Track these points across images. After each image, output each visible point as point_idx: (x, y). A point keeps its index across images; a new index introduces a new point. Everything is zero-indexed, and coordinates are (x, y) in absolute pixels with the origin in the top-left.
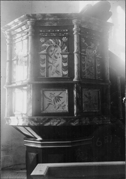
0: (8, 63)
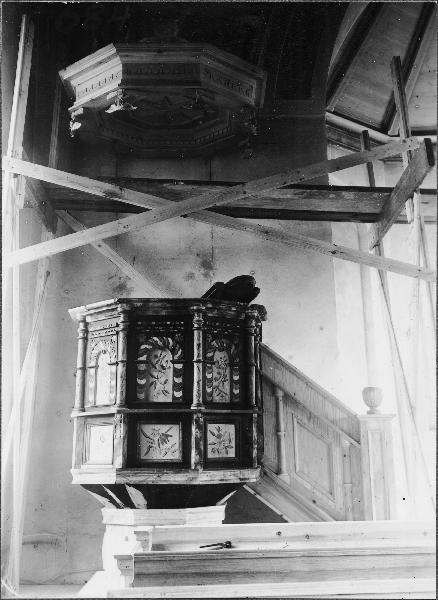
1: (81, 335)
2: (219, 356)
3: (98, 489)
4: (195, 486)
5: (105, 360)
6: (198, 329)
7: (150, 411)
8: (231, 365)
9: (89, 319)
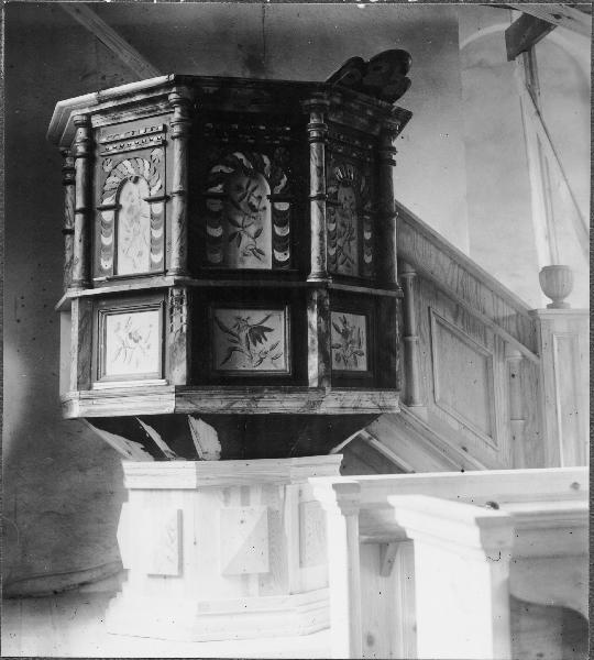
0: (79, 218)
1: (81, 149)
2: (344, 195)
3: (127, 427)
4: (316, 416)
5: (134, 195)
6: (318, 140)
7: (229, 283)
8: (360, 212)
9: (97, 121)
